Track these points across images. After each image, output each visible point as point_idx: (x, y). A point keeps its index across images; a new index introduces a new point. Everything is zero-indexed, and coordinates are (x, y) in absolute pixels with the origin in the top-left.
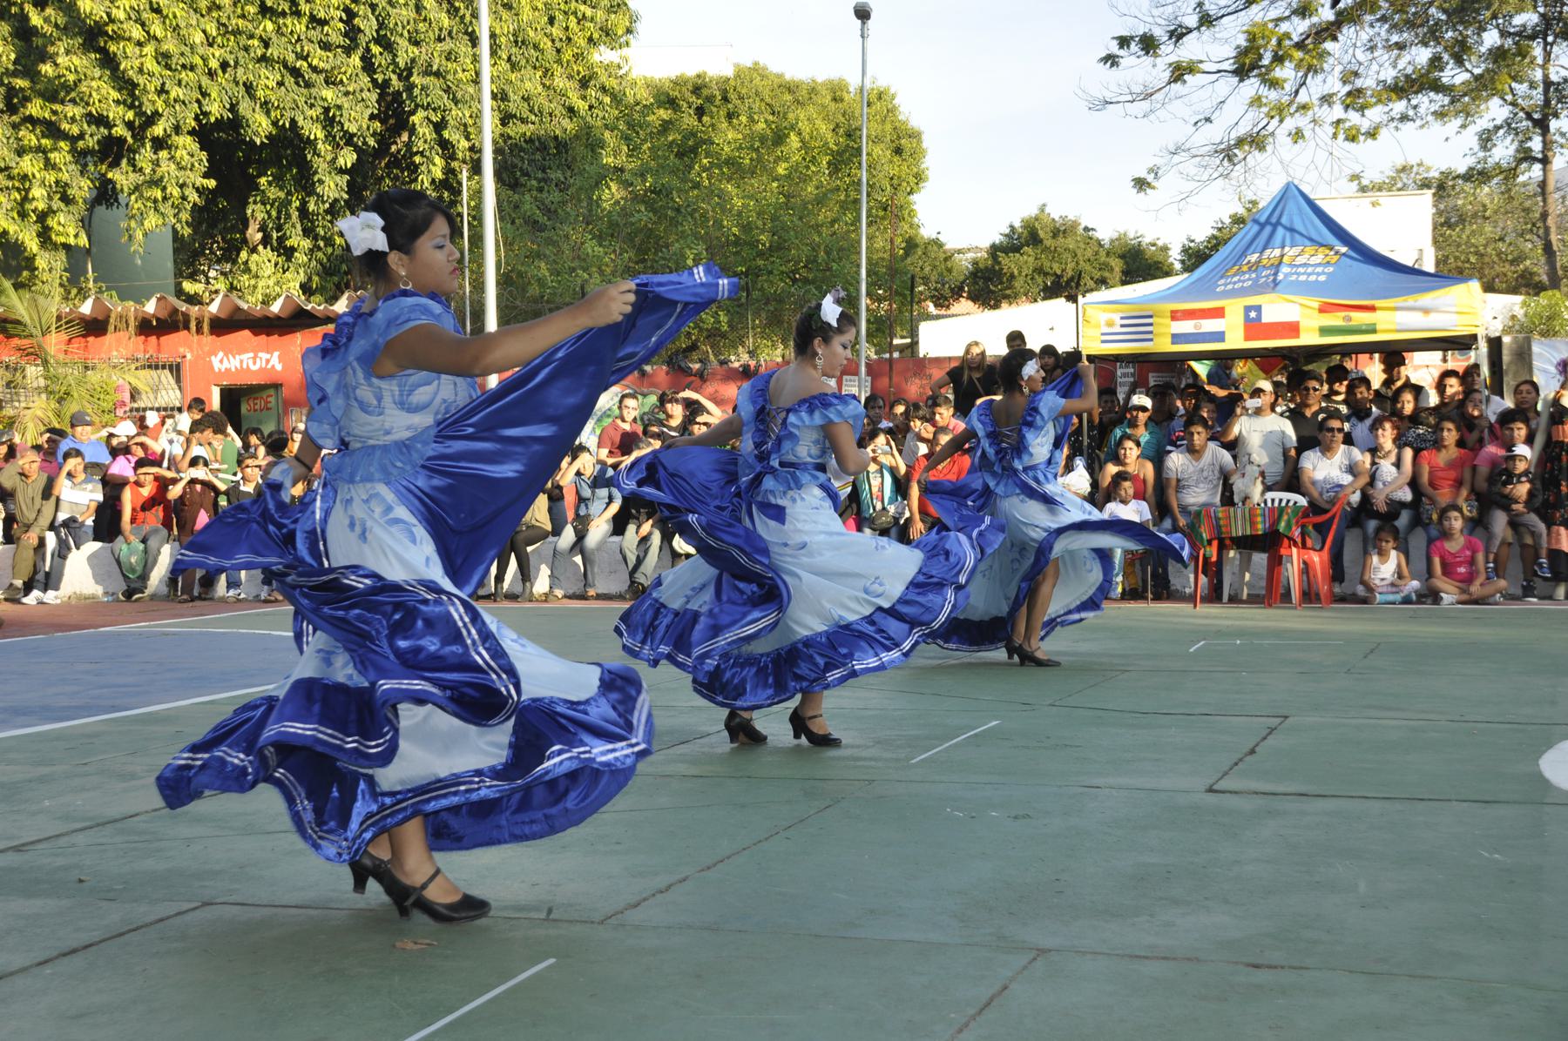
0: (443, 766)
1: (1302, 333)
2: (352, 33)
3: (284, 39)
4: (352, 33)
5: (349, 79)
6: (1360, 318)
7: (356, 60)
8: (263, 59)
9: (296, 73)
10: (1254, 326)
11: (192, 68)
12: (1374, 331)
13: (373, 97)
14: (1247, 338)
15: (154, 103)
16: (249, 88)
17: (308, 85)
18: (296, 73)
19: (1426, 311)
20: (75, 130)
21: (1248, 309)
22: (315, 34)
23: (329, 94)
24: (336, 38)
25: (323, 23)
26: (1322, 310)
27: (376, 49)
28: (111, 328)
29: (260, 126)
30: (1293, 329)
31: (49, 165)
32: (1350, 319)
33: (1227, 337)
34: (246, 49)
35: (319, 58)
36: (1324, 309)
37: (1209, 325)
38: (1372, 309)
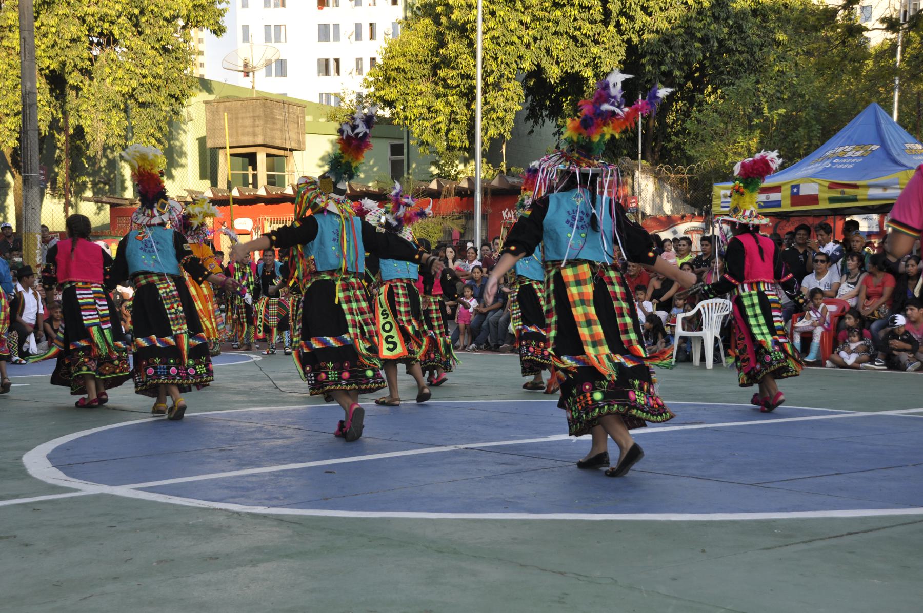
0: (367, 400)
1: (820, 202)
2: (607, 13)
3: (567, 20)
4: (607, 13)
5: (608, 40)
6: (850, 192)
7: (611, 28)
8: (556, 33)
9: (574, 38)
10: (797, 198)
11: (512, 43)
12: (856, 200)
13: (622, 50)
14: (793, 205)
15: (491, 65)
16: (548, 51)
17: (583, 45)
18: (574, 38)
19: (885, 187)
20: (455, 83)
21: (793, 187)
22: (585, 15)
23: (595, 50)
24: (599, 17)
25: (589, 8)
26: (830, 188)
27: (623, 20)
28: (442, 196)
29: (554, 73)
30: (814, 199)
31: (448, 103)
32: (843, 193)
33: (782, 203)
34: (547, 28)
35: (587, 28)
36: (833, 186)
37: (774, 197)
38: (855, 186)
